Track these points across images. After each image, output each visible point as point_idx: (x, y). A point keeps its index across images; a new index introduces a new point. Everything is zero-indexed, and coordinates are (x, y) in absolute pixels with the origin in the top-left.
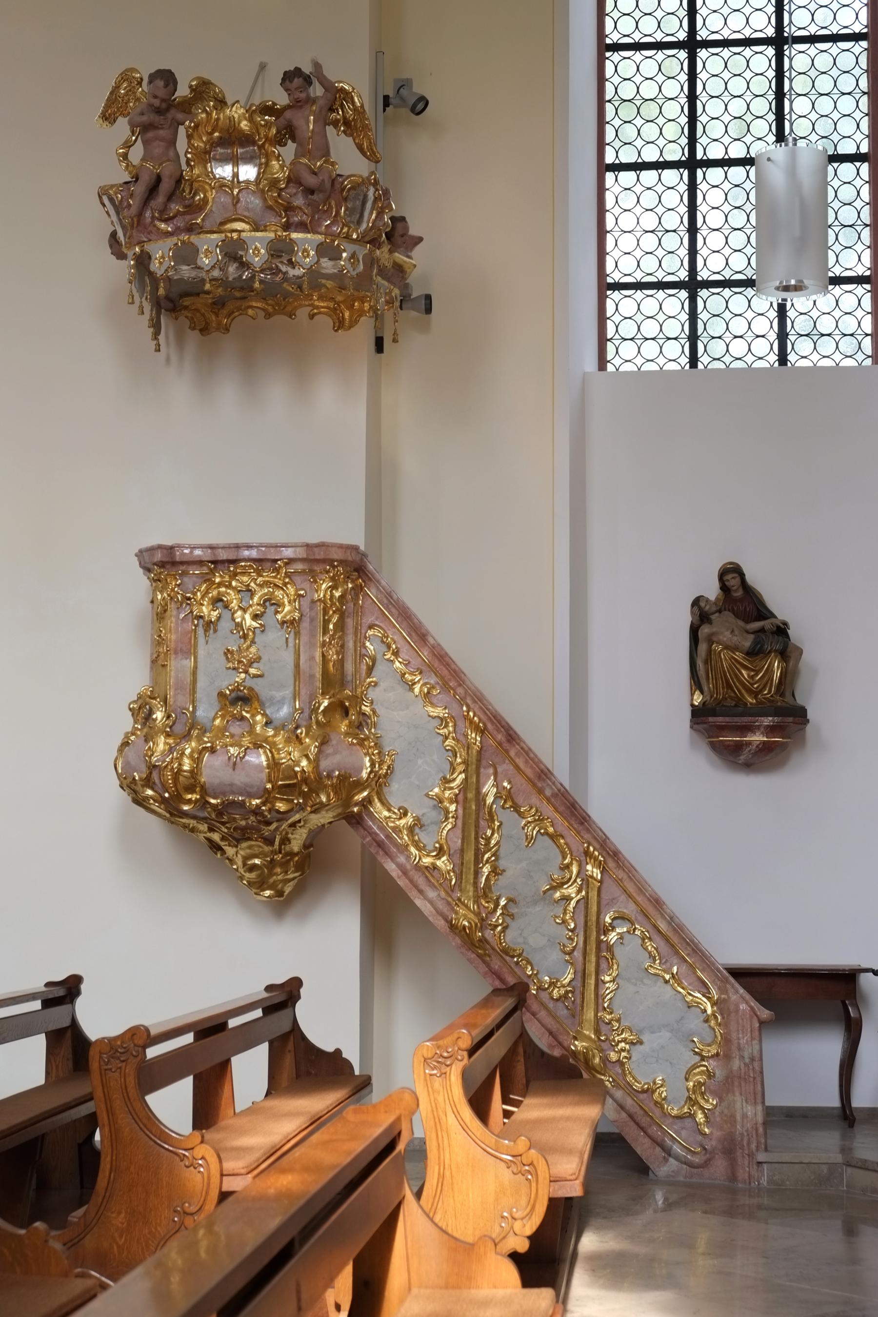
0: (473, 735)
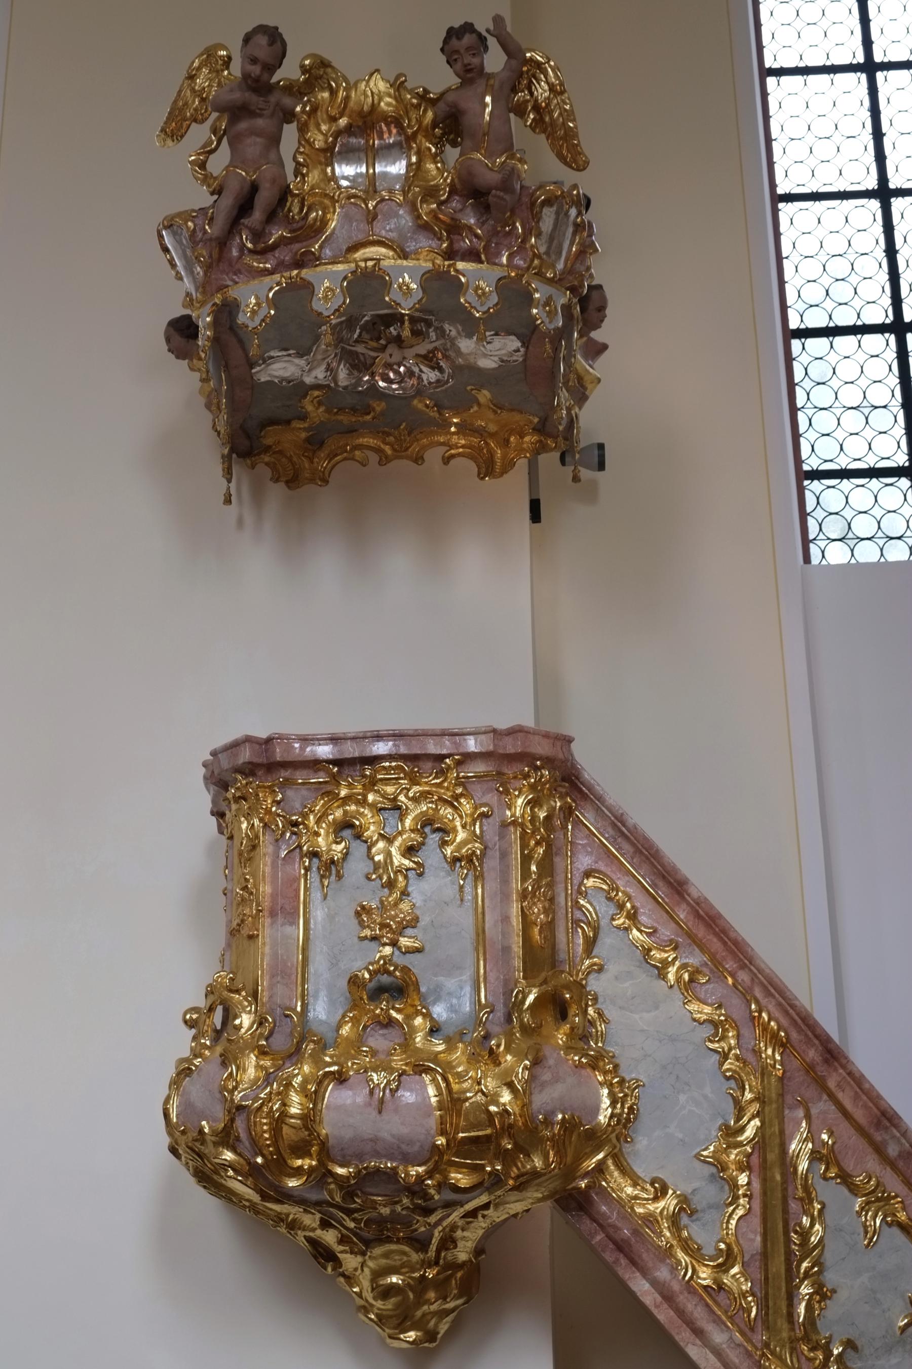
0: (770, 1052)
